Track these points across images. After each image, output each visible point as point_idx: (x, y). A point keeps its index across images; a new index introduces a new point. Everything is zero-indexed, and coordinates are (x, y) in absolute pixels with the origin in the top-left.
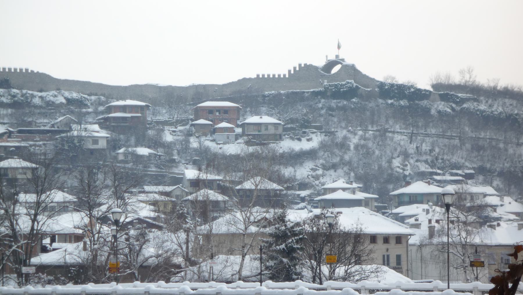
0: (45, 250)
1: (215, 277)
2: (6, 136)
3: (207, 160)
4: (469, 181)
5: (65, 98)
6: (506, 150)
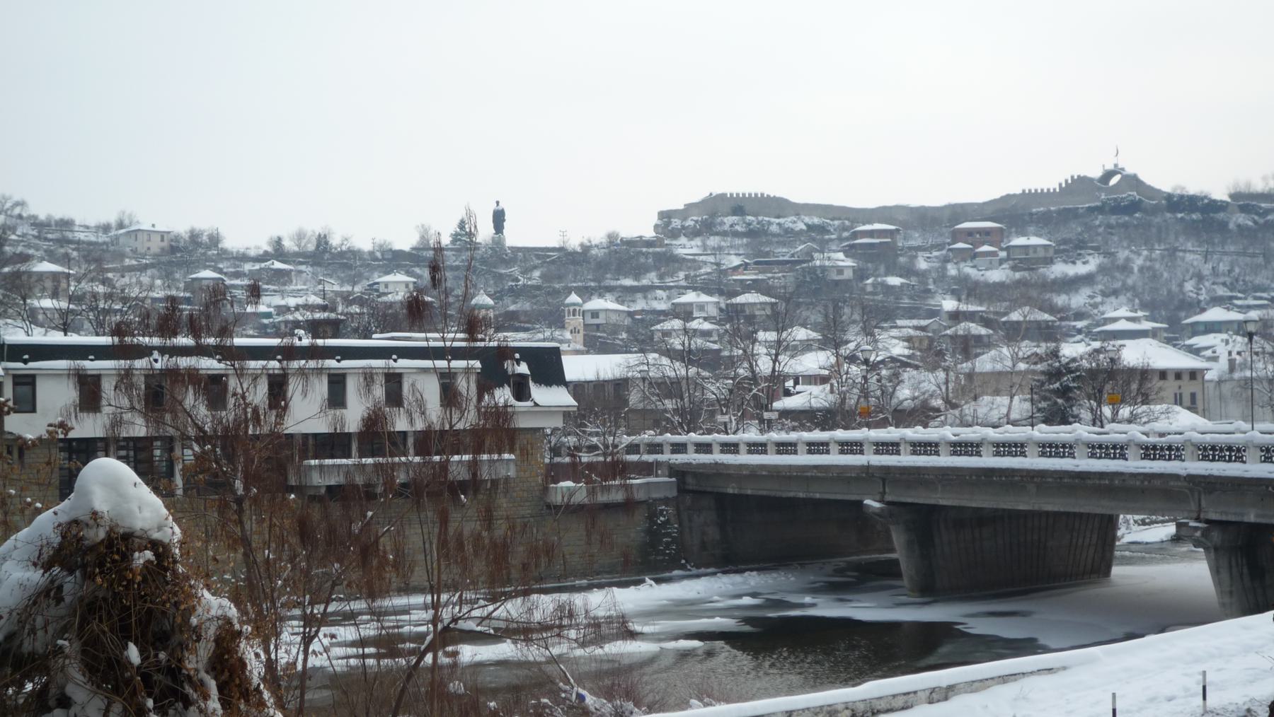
0: (788, 393)
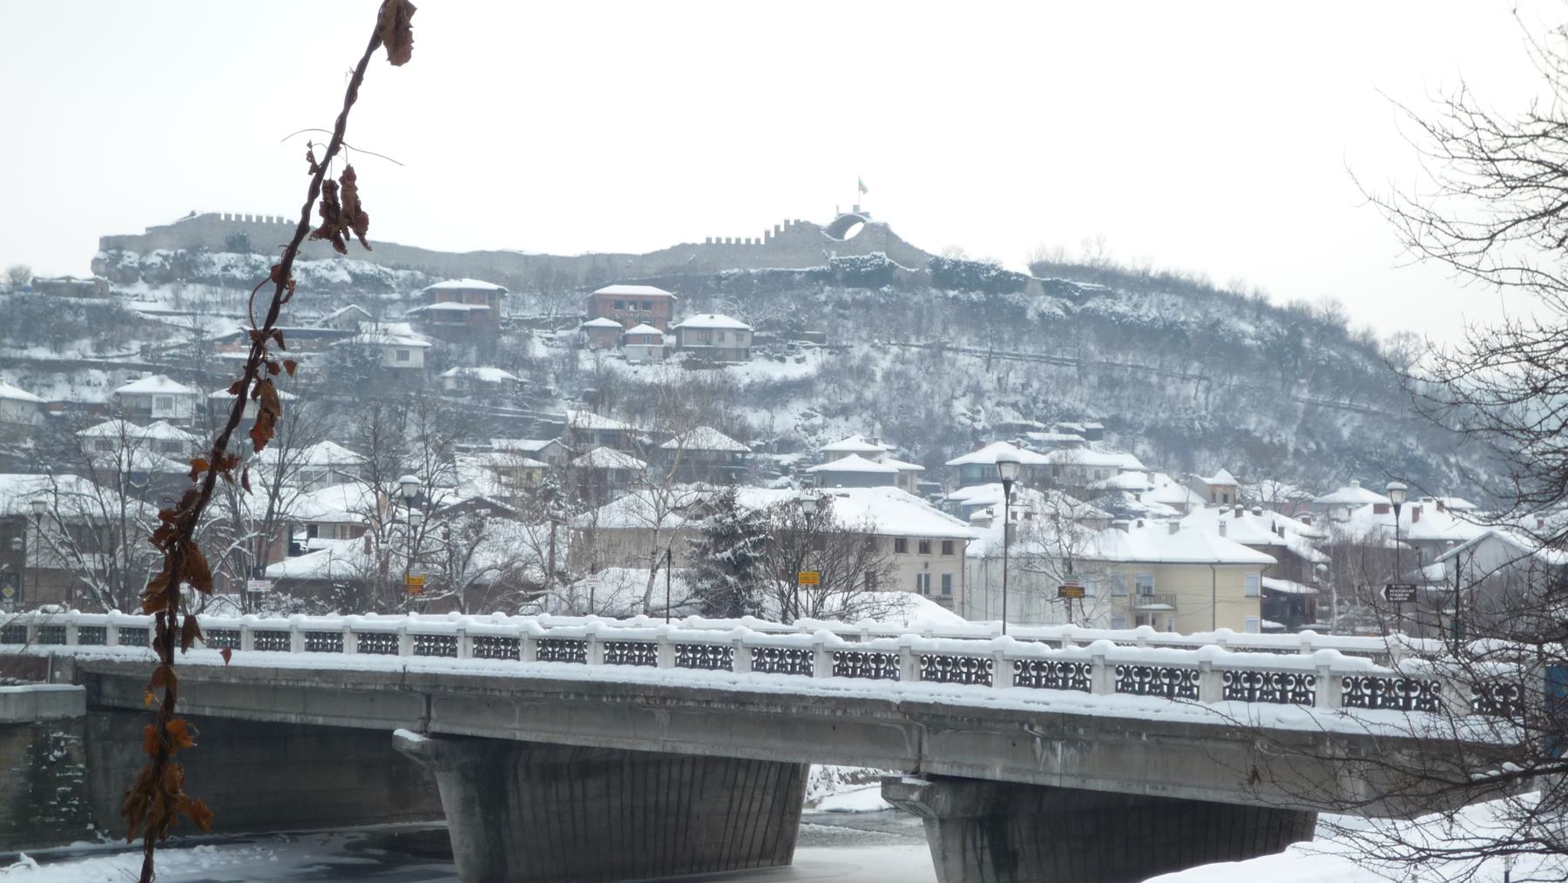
0: (295, 551)
1: (601, 607)
2: (238, 340)
3: (602, 392)
4: (1092, 443)
5: (349, 273)
6: (1162, 388)
